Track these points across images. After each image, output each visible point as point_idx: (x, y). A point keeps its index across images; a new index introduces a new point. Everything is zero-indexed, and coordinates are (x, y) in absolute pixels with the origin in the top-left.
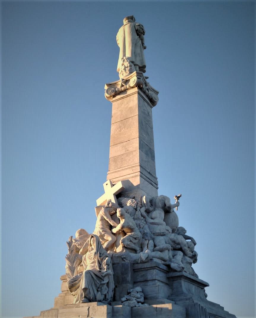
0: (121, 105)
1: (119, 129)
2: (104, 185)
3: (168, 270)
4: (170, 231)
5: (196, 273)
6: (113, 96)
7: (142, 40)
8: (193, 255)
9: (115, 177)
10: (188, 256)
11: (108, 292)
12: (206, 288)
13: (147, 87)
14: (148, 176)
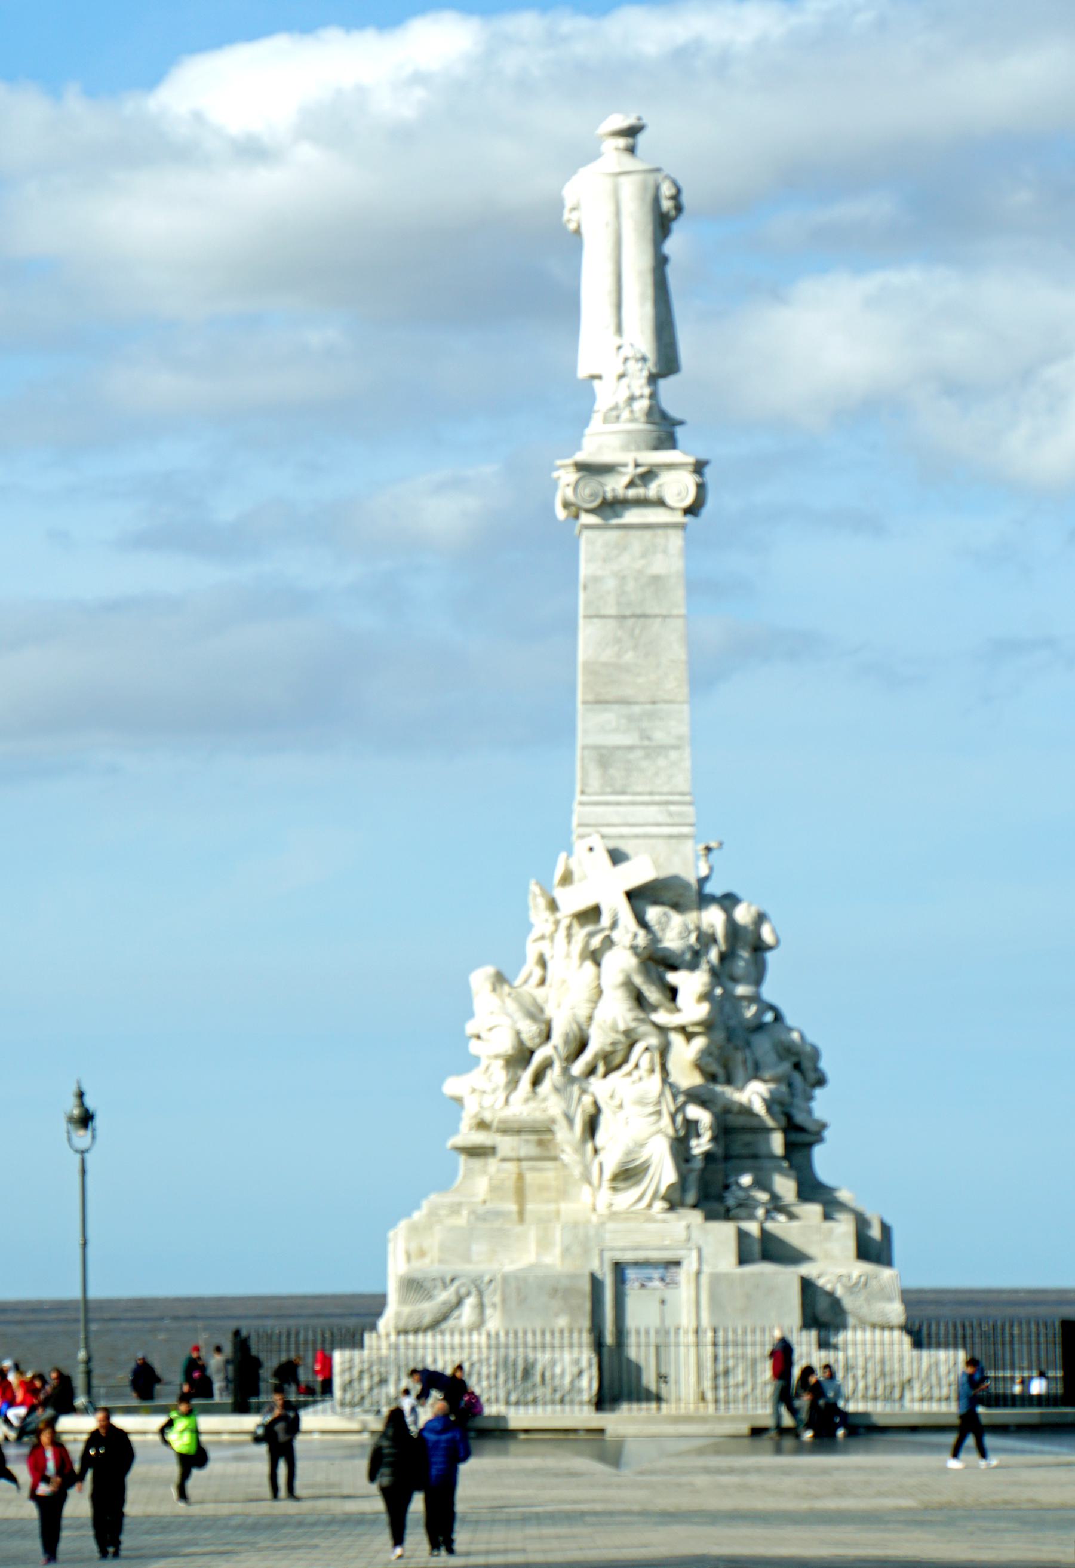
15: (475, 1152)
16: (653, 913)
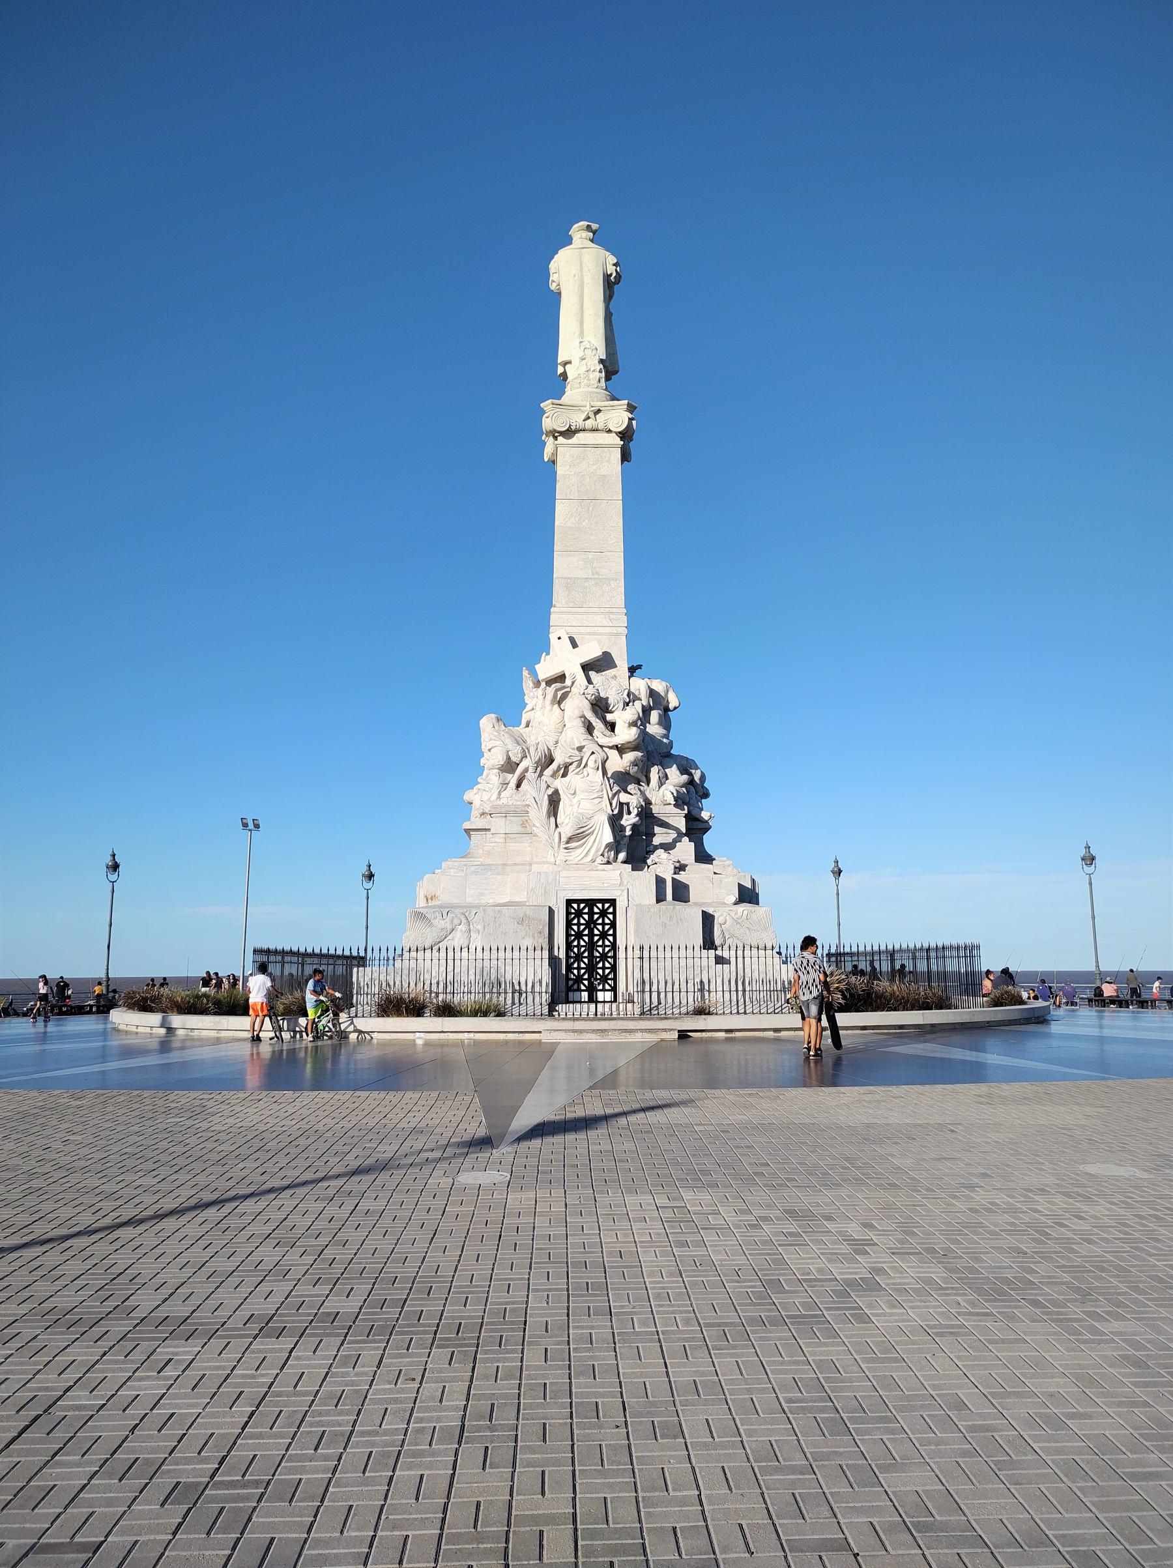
15: (420, 916)
16: (592, 674)
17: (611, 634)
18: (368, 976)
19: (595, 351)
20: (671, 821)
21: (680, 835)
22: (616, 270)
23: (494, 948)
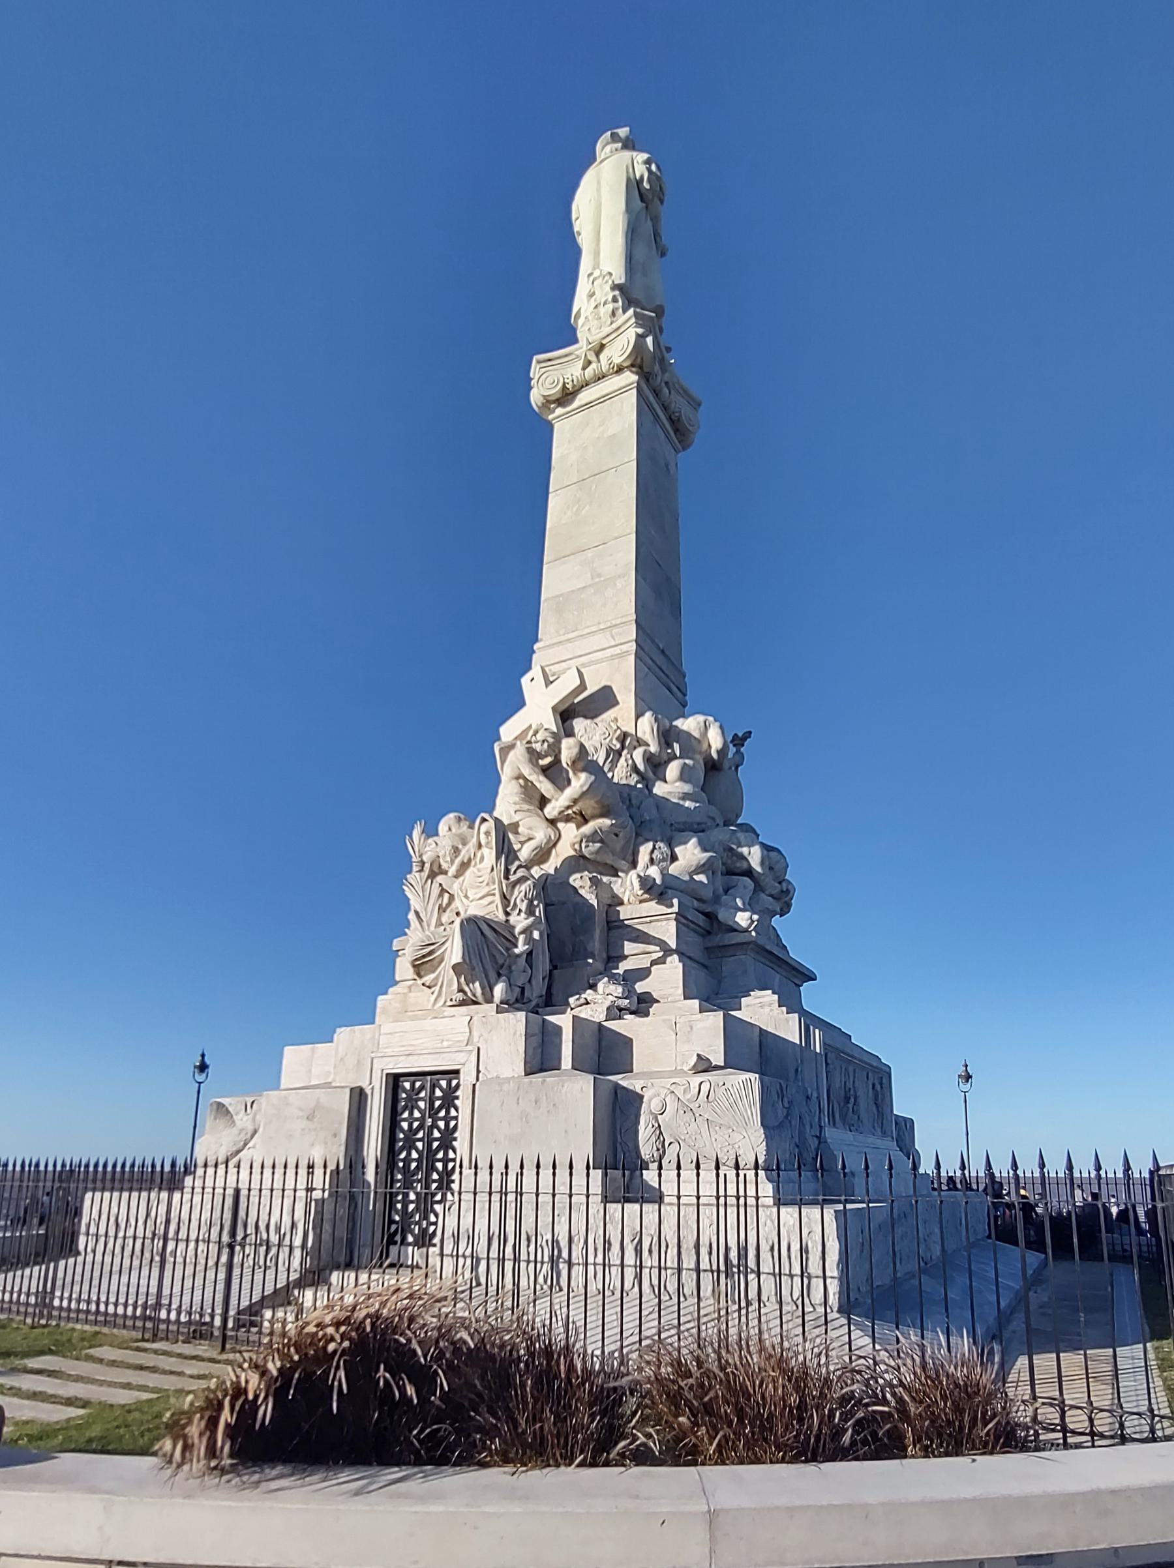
0: (583, 430)
1: (574, 509)
2: (525, 681)
3: (708, 929)
4: (718, 821)
5: (52, 1369)
6: (557, 400)
7: (655, 220)
8: (782, 891)
9: (557, 660)
10: (767, 892)
11: (530, 981)
12: (806, 988)
13: (667, 377)
14: (660, 659)
17: (613, 657)
18: (207, 1210)
19: (607, 278)
20: (651, 930)
21: (667, 951)
22: (649, 170)
23: (547, 1163)
